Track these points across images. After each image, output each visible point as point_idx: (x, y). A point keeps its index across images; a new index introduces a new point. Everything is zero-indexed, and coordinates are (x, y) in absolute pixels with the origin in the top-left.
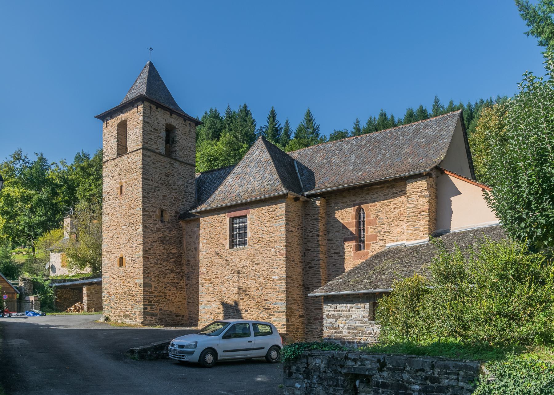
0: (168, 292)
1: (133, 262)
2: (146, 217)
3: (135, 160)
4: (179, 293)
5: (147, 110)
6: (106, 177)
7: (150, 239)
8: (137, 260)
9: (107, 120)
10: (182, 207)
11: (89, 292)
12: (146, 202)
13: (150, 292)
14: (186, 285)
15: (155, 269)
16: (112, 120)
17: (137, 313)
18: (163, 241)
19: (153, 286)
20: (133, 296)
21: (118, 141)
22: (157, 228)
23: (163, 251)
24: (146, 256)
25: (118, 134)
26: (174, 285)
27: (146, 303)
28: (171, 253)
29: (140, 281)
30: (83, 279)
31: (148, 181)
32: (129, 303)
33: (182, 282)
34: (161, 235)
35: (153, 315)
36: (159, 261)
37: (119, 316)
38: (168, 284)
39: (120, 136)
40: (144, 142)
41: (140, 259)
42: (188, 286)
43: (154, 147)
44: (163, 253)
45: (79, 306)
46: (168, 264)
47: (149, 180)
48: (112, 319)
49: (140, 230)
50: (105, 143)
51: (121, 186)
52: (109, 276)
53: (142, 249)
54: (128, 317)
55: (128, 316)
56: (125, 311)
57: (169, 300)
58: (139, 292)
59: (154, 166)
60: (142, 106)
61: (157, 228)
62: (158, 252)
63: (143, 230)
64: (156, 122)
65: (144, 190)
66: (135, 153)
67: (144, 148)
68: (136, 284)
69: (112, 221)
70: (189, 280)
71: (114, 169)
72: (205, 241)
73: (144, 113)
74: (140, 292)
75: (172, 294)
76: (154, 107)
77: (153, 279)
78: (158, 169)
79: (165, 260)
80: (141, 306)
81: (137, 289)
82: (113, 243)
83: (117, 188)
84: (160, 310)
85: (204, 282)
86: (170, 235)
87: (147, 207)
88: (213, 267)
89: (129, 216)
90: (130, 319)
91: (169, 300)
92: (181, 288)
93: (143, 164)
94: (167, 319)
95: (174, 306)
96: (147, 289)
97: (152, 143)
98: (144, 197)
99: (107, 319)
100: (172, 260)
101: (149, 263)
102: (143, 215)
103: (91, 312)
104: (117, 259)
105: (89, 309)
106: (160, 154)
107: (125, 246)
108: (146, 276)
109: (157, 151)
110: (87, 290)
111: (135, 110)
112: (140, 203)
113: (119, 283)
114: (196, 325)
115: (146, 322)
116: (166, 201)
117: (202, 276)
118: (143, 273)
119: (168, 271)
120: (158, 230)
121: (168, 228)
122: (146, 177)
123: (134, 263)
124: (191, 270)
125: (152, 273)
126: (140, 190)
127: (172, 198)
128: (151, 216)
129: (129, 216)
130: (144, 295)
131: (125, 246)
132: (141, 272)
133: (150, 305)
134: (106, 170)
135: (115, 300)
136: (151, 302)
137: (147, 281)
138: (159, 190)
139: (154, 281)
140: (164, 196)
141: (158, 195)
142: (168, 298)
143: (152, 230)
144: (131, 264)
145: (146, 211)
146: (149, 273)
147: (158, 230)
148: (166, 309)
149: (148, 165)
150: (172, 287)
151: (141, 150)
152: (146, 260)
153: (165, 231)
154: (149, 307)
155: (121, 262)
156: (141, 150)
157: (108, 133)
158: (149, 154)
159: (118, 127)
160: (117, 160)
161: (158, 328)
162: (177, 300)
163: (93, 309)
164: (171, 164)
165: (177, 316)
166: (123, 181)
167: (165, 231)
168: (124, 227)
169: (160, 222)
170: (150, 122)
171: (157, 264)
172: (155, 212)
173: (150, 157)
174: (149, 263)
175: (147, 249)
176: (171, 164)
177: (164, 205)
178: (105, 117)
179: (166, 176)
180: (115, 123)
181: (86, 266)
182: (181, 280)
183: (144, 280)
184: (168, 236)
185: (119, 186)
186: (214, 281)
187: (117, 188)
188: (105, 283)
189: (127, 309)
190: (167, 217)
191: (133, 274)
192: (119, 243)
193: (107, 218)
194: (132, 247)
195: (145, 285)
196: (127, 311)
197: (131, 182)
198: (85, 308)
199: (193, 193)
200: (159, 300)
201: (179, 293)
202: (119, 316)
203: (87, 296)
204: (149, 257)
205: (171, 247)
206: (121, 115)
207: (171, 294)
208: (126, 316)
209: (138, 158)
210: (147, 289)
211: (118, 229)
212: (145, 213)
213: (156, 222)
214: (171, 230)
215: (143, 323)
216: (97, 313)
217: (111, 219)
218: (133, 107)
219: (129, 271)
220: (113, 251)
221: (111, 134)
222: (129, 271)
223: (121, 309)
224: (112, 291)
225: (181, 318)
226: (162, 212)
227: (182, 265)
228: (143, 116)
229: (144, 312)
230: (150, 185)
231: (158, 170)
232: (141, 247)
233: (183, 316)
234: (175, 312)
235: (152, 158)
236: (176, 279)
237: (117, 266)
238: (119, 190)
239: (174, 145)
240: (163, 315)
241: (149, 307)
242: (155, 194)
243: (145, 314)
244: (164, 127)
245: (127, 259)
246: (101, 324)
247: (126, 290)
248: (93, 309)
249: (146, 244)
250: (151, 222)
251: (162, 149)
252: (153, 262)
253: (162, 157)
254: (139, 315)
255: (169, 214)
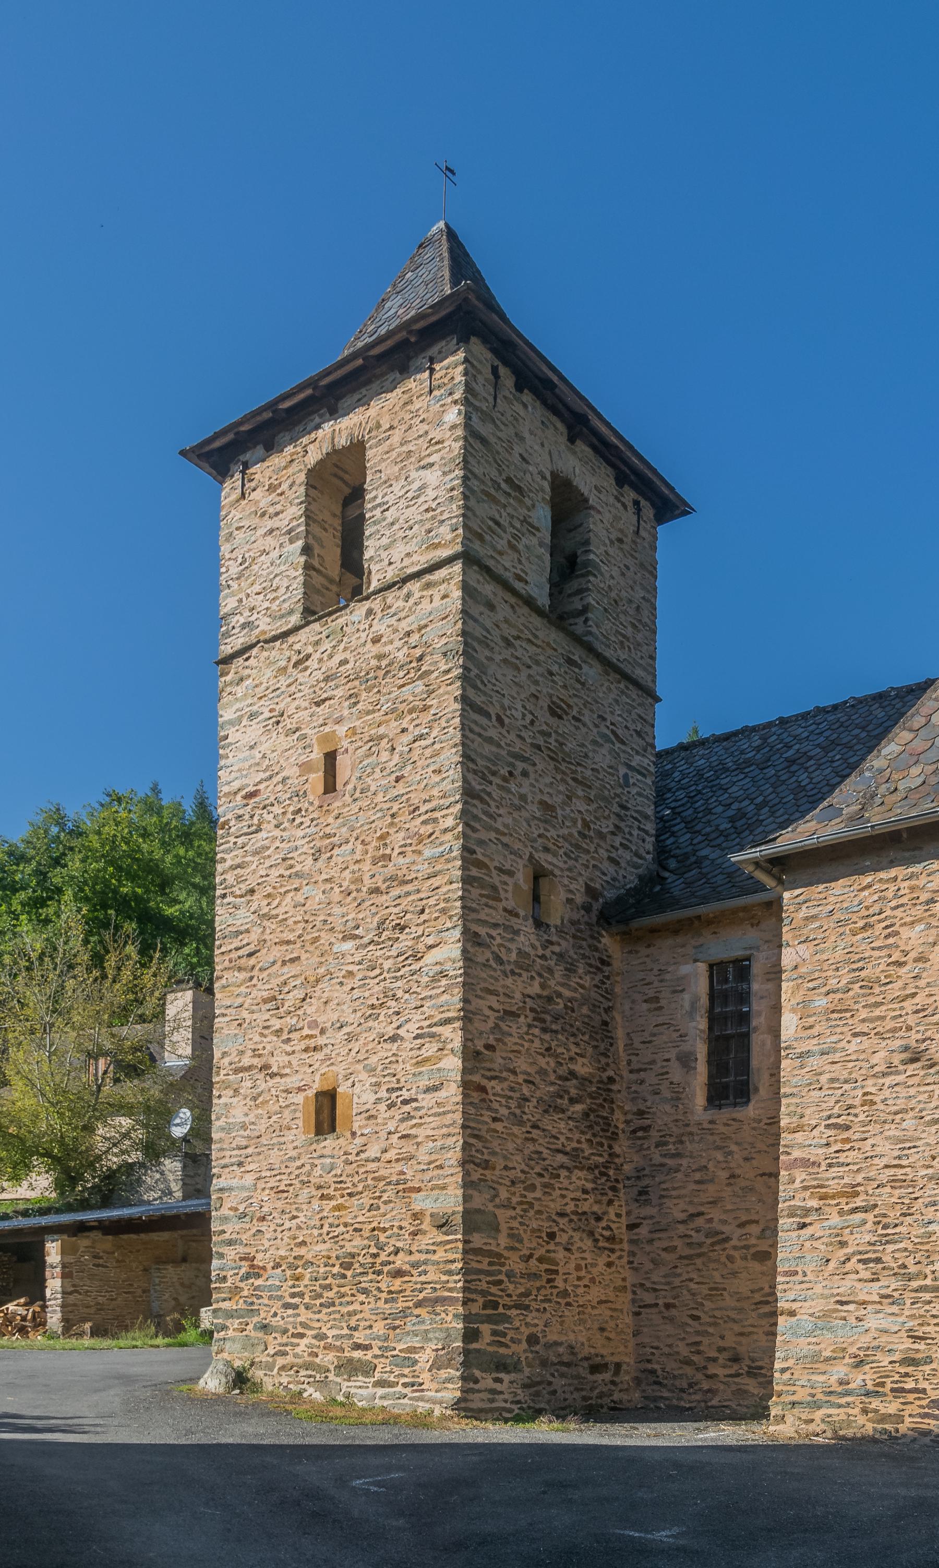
0: (561, 1255)
1: (397, 1113)
2: (475, 892)
3: (418, 615)
4: (602, 1261)
5: (480, 379)
6: (231, 723)
7: (493, 1001)
8: (427, 1101)
9: (246, 466)
10: (611, 869)
11: (70, 1259)
12: (475, 817)
13: (490, 1253)
14: (631, 1227)
15: (511, 1146)
16: (277, 460)
17: (425, 1358)
18: (544, 1014)
19: (504, 1227)
20: (399, 1273)
21: (306, 550)
22: (520, 952)
23: (542, 1062)
24: (476, 1078)
25: (309, 516)
26: (587, 1222)
27: (475, 1308)
28: (572, 1074)
29: (451, 1200)
30: (25, 1213)
31: (484, 721)
32: (365, 1307)
33: (612, 1211)
34: (535, 989)
35: (502, 1366)
36: (530, 1107)
37: (307, 1366)
38: (563, 1221)
39: (316, 529)
40: (473, 530)
41: (442, 1094)
42: (643, 1231)
43: (507, 565)
44: (542, 1072)
45: (21, 1311)
46: (559, 1126)
47: (487, 715)
48: (271, 1381)
49: (449, 951)
50: (234, 570)
51: (330, 758)
52: (249, 1179)
53: (457, 1043)
54: (367, 1374)
55: (367, 1369)
56: (347, 1344)
57: (565, 1294)
58: (440, 1261)
59: (507, 654)
60: (461, 355)
61: (520, 952)
62: (522, 1064)
63: (464, 951)
64: (517, 449)
65: (467, 758)
66: (414, 587)
67: (467, 557)
68: (415, 1216)
69: (270, 925)
70: (647, 1202)
71: (283, 682)
72: (821, 1002)
73: (469, 389)
74: (440, 1255)
75: (578, 1268)
76: (508, 379)
77: (504, 1194)
78: (525, 672)
79: (550, 1107)
80: (451, 1320)
81: (424, 1241)
82: (276, 1024)
83: (306, 767)
84: (532, 1340)
85: (814, 1203)
86: (567, 993)
87: (481, 843)
88: (873, 1128)
89: (376, 891)
90: (381, 1384)
91: (565, 1294)
92: (611, 1239)
93: (464, 633)
94: (559, 1383)
95: (582, 1322)
96: (478, 1240)
97: (502, 544)
98: (468, 793)
99: (240, 1379)
100: (579, 1108)
101: (487, 1116)
102: (467, 880)
103: (81, 1335)
104: (299, 1098)
105: (69, 1326)
106: (529, 602)
107: (350, 1038)
108: (475, 1177)
109: (518, 585)
110: (63, 1252)
111: (417, 383)
112: (450, 822)
113: (310, 1210)
114: (760, 1413)
115: (477, 1402)
116: (552, 833)
117: (800, 1176)
118: (463, 1163)
119: (561, 1159)
120: (524, 964)
121: (561, 956)
122: (479, 700)
123: (409, 1117)
124: (657, 1159)
125: (501, 1163)
126: (451, 756)
127: (574, 822)
128: (494, 888)
129: (376, 891)
130: (466, 1271)
131: (350, 1038)
132: (453, 1156)
133: (489, 1319)
134: (240, 690)
135: (286, 1290)
136: (495, 1305)
137: (478, 1201)
138: (525, 774)
139: (507, 1206)
140: (544, 805)
141: (523, 797)
142: (559, 1283)
143: (498, 959)
144: (390, 1120)
145: (480, 865)
146: (486, 1165)
147: (524, 964)
148: (552, 1337)
149: (484, 642)
150: (577, 1236)
151: (457, 567)
152: (476, 1096)
153: (550, 971)
154: (486, 1329)
155: (326, 1113)
156: (457, 567)
157: (256, 521)
158: (488, 589)
159: (309, 485)
160: (303, 635)
161: (545, 1432)
162: (596, 1293)
163: (88, 1326)
164: (570, 662)
165: (595, 1369)
166: (341, 730)
167: (550, 971)
168: (348, 946)
169: (528, 927)
170: (492, 440)
171: (521, 1123)
172: (510, 873)
173: (491, 607)
174: (487, 1116)
175: (479, 1045)
176: (570, 662)
177: (546, 849)
178: (227, 453)
179: (553, 713)
180: (294, 467)
181: (28, 1168)
182: (610, 1202)
183: (466, 1198)
184: (559, 995)
185: (317, 755)
186: (886, 1196)
187: (306, 767)
188: (225, 1211)
189: (360, 1337)
190: (558, 910)
191: (398, 1167)
192: (313, 1024)
193: (242, 912)
194: (394, 1039)
195: (473, 1221)
196: (357, 1347)
197: (393, 727)
198: (54, 1319)
199: (647, 817)
200: (527, 1294)
201: (602, 1261)
202: (307, 1366)
203: (64, 1276)
204: (489, 1085)
205: (574, 1049)
206: (327, 427)
207: (572, 1265)
208: (350, 1368)
209: (440, 606)
210: (478, 1240)
211: (309, 960)
212: (474, 872)
213: (515, 922)
214: (571, 970)
215: (464, 1408)
216: (107, 1342)
217: (268, 917)
218: (405, 370)
219: (373, 1151)
220: (275, 1064)
221: (270, 524)
222: (373, 1151)
223: (321, 1337)
224: (271, 1248)
225: (607, 1376)
226: (539, 875)
227: (614, 1137)
228: (466, 402)
229: (466, 1352)
230: (490, 740)
231: (523, 677)
232: (453, 1036)
233: (618, 1366)
234: (586, 1351)
235: (500, 616)
236: (591, 1198)
237: (299, 1134)
238: (317, 778)
239: (574, 585)
240: (544, 1363)
241: (486, 1329)
242: (512, 787)
243: (477, 1359)
244: (546, 485)
245: (359, 1094)
246: (210, 1401)
247: (355, 1244)
248: (88, 1326)
249: (478, 1024)
250: (498, 916)
251: (538, 587)
252: (504, 1111)
253: (537, 621)
254: (437, 1365)
255: (563, 895)
